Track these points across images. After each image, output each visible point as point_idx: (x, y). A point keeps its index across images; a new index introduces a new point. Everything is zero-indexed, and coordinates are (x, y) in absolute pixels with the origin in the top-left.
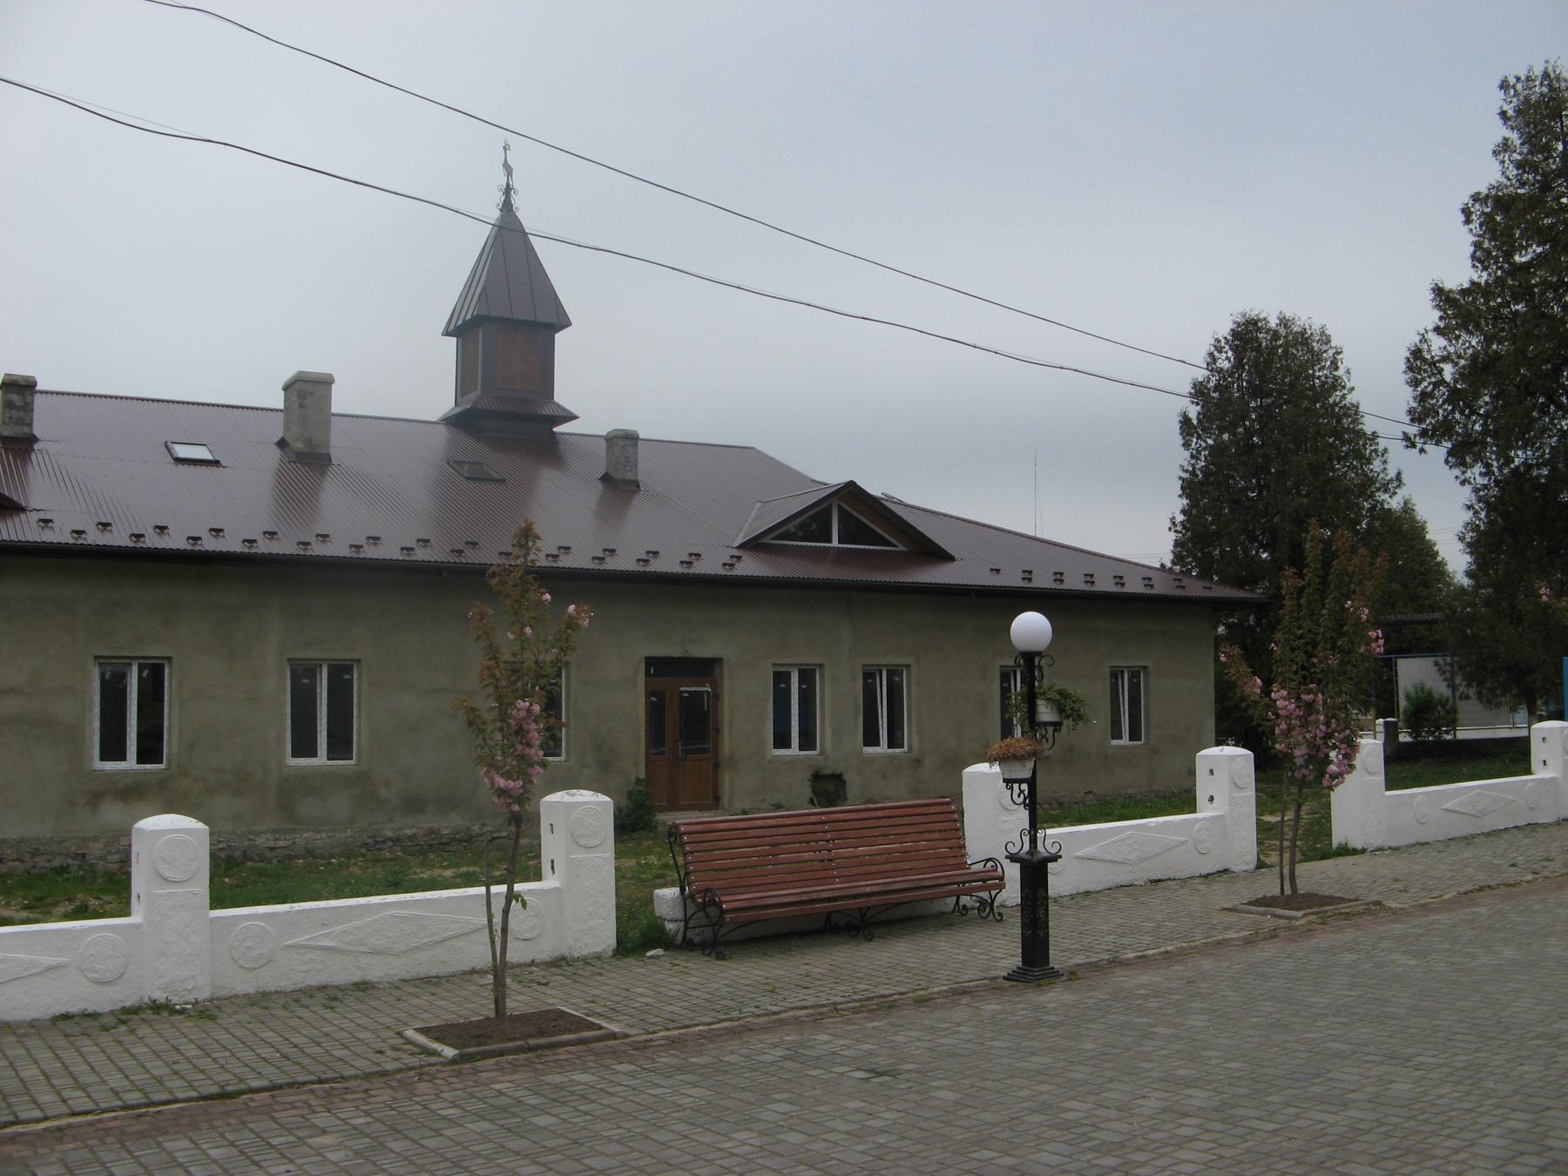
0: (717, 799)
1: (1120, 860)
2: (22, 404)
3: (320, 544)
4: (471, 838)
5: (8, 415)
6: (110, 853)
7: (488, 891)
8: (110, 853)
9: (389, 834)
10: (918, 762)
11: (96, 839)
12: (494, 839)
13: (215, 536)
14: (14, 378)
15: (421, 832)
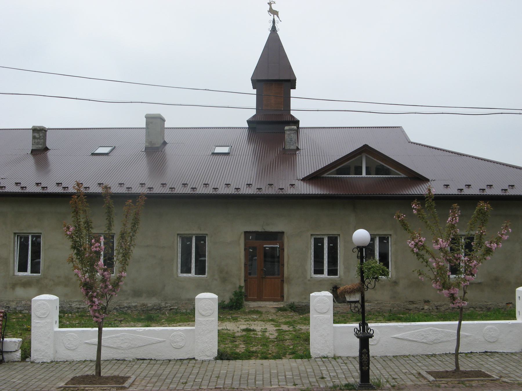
0: (282, 297)
1: (115, 347)
2: (39, 137)
3: (467, 189)
4: (161, 308)
5: (34, 141)
6: (18, 306)
7: (460, 324)
8: (18, 306)
9: (126, 305)
10: (395, 283)
11: (13, 301)
12: (171, 309)
13: (468, 188)
14: (35, 127)
15: (139, 305)
